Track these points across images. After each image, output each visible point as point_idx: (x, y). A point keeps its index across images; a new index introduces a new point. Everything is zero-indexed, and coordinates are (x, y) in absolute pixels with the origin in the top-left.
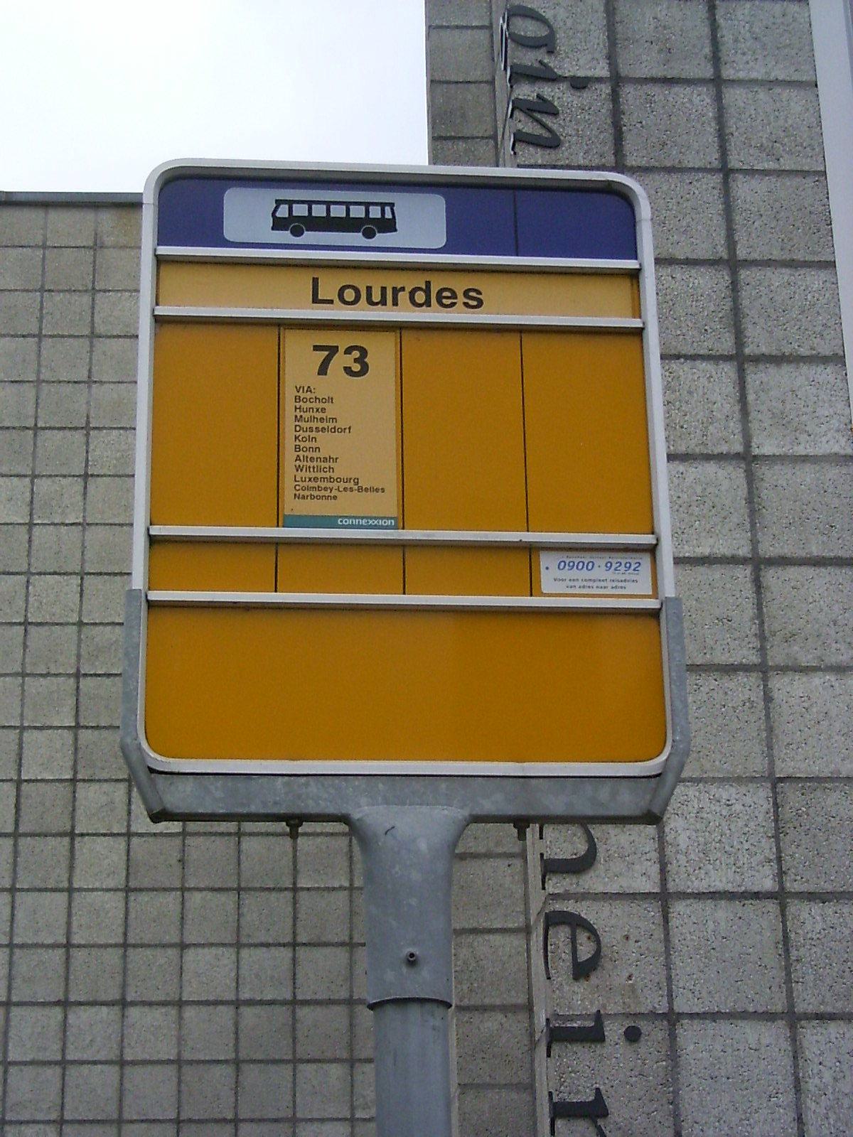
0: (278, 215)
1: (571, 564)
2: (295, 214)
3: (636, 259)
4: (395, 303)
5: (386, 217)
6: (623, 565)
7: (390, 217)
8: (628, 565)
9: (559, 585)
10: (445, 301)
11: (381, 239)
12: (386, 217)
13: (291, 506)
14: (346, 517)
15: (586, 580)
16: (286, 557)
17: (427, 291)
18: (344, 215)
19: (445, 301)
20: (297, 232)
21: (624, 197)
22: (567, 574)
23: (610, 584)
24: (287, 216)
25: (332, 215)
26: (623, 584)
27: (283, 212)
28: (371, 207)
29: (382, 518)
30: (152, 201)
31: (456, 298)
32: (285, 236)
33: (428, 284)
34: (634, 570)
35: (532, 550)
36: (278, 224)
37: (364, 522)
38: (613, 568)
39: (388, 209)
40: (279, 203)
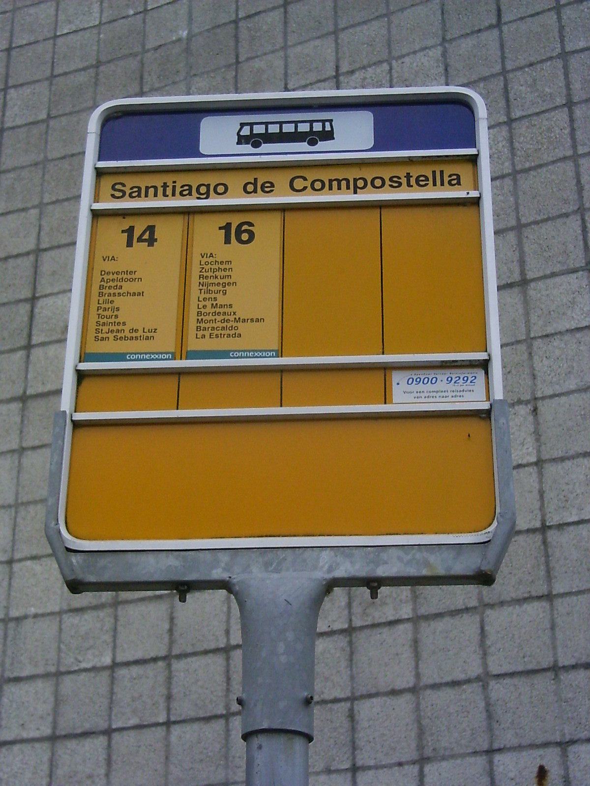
0: (241, 134)
1: (418, 380)
2: (255, 132)
3: (475, 147)
4: (146, 196)
5: (326, 129)
6: (462, 379)
7: (330, 129)
8: (466, 379)
9: (406, 396)
10: (421, 183)
11: (322, 145)
12: (326, 129)
13: (194, 344)
14: (236, 351)
15: (430, 392)
16: (185, 381)
17: (255, 184)
18: (293, 130)
19: (421, 183)
20: (256, 145)
21: (464, 104)
22: (414, 387)
23: (451, 394)
24: (249, 134)
25: (284, 131)
26: (461, 394)
27: (246, 131)
28: (284, 125)
29: (162, 353)
30: (480, 122)
31: (428, 181)
32: (248, 148)
33: (256, 179)
34: (471, 382)
35: (387, 368)
36: (241, 140)
37: (147, 356)
38: (453, 381)
39: (327, 124)
40: (242, 125)
